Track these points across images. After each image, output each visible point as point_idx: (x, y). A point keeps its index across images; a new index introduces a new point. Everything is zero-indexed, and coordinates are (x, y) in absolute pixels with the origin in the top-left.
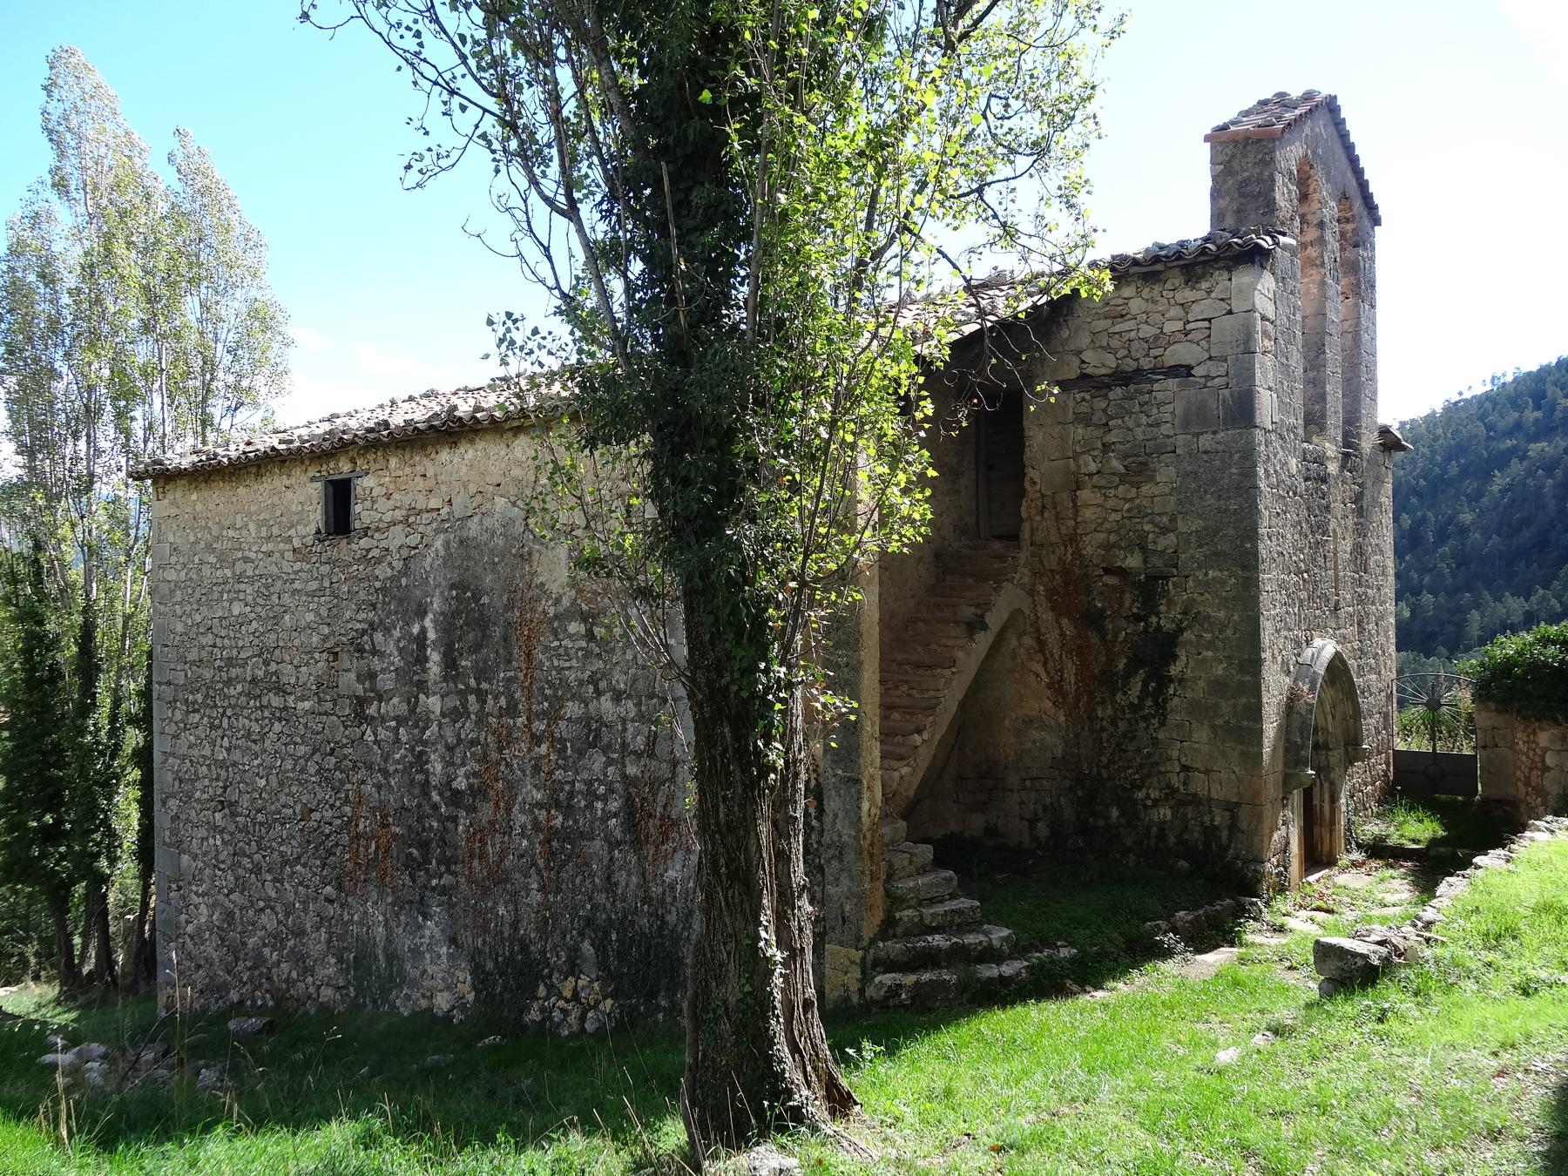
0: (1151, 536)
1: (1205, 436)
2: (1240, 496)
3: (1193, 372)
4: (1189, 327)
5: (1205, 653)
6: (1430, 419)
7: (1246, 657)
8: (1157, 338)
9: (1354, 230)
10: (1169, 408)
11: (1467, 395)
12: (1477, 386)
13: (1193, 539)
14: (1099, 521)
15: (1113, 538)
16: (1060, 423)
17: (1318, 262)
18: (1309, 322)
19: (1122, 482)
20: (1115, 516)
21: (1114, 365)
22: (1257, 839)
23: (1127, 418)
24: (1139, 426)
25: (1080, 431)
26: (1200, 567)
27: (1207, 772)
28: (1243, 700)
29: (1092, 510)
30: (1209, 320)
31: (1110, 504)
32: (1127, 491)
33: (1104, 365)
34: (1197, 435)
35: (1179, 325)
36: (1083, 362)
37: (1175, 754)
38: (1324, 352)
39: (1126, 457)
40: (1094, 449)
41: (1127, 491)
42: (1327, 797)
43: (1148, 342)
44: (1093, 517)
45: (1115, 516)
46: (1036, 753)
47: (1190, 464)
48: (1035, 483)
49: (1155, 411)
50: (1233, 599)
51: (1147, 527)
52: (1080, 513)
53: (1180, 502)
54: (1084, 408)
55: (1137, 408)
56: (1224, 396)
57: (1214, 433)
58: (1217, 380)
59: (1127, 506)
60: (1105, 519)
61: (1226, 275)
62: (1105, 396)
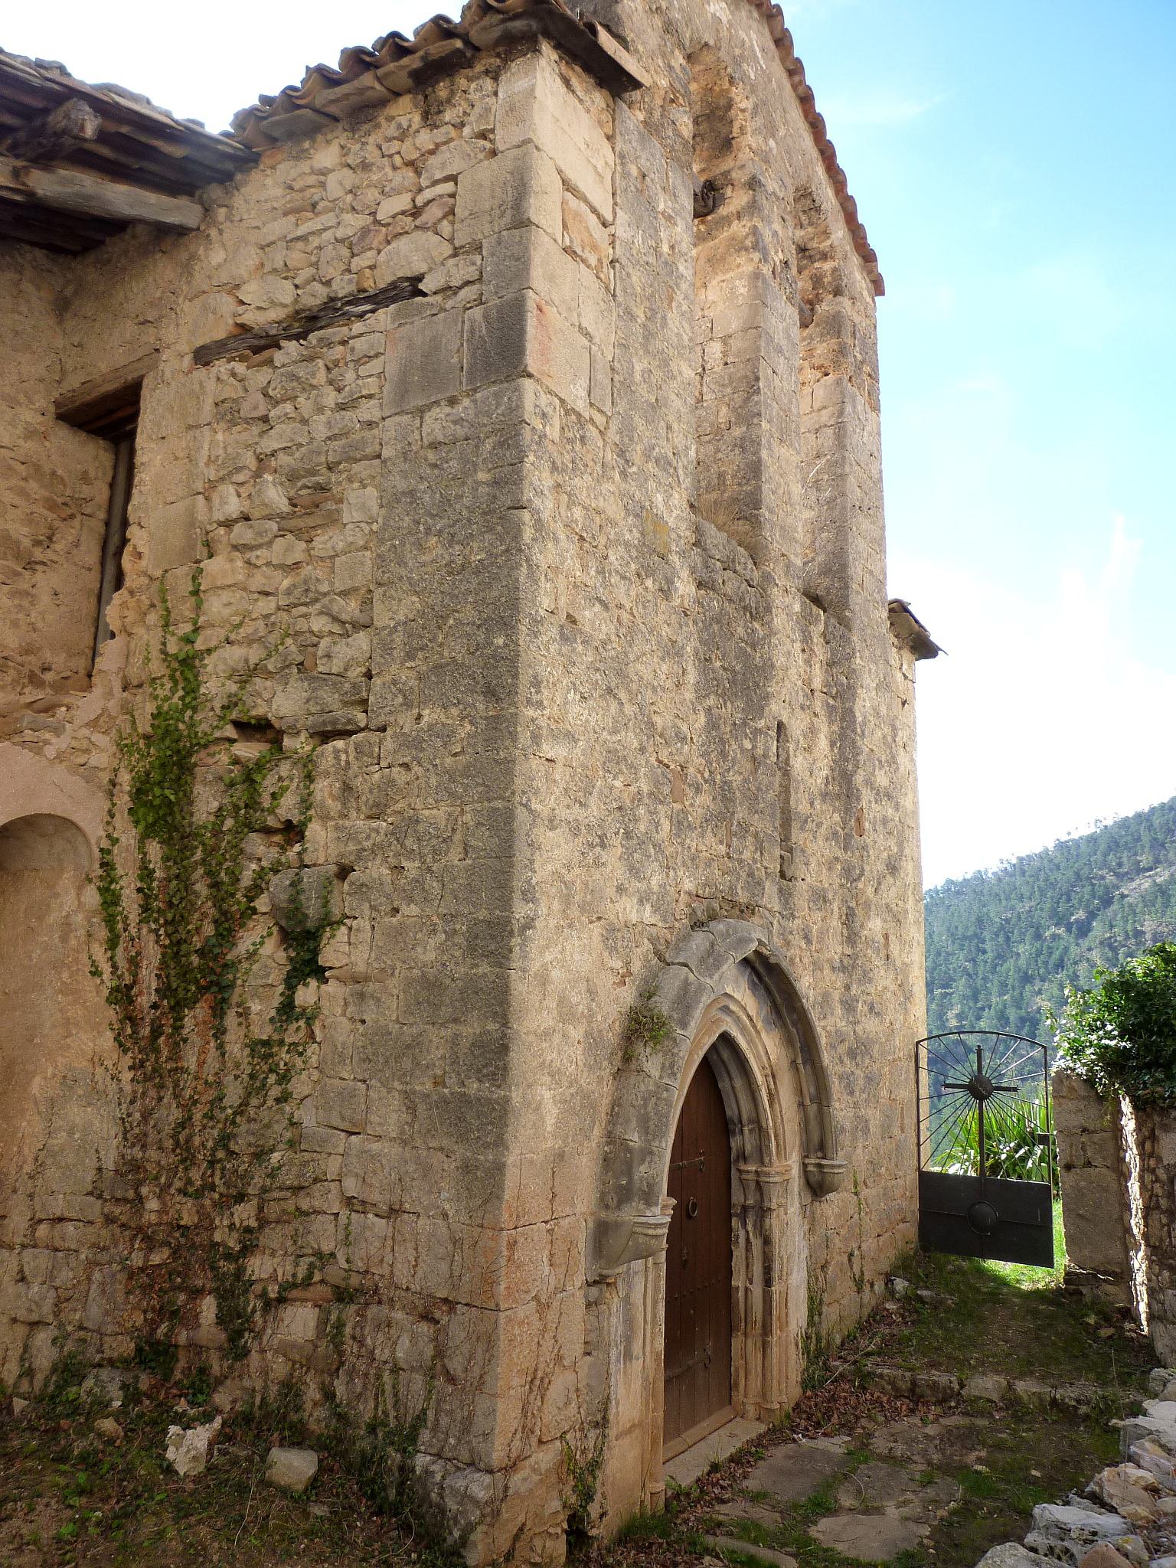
0: (324, 643)
1: (436, 410)
2: (491, 530)
3: (421, 286)
4: (420, 200)
5: (405, 910)
6: (1044, 856)
7: (482, 914)
8: (365, 232)
9: (835, 270)
10: (375, 366)
11: (1075, 836)
12: (1080, 826)
13: (399, 638)
14: (237, 620)
15: (255, 654)
16: (190, 427)
17: (748, 243)
18: (736, 344)
19: (282, 533)
20: (267, 605)
21: (288, 299)
22: (482, 1404)
23: (301, 400)
24: (320, 410)
25: (220, 436)
26: (408, 704)
27: (393, 1212)
28: (470, 1029)
29: (226, 596)
30: (453, 178)
31: (258, 581)
32: (289, 549)
33: (273, 303)
34: (421, 411)
35: (403, 202)
36: (242, 303)
37: (333, 1167)
38: (758, 392)
39: (293, 477)
40: (239, 470)
41: (289, 549)
42: (757, 1269)
43: (353, 246)
44: (226, 612)
45: (267, 605)
46: (71, 1158)
47: (404, 474)
48: (139, 555)
49: (350, 376)
50: (466, 772)
51: (319, 624)
52: (205, 605)
53: (381, 561)
54: (232, 390)
55: (322, 376)
56: (472, 321)
57: (452, 402)
58: (463, 293)
59: (286, 583)
60: (246, 615)
61: (488, 84)
62: (270, 362)
